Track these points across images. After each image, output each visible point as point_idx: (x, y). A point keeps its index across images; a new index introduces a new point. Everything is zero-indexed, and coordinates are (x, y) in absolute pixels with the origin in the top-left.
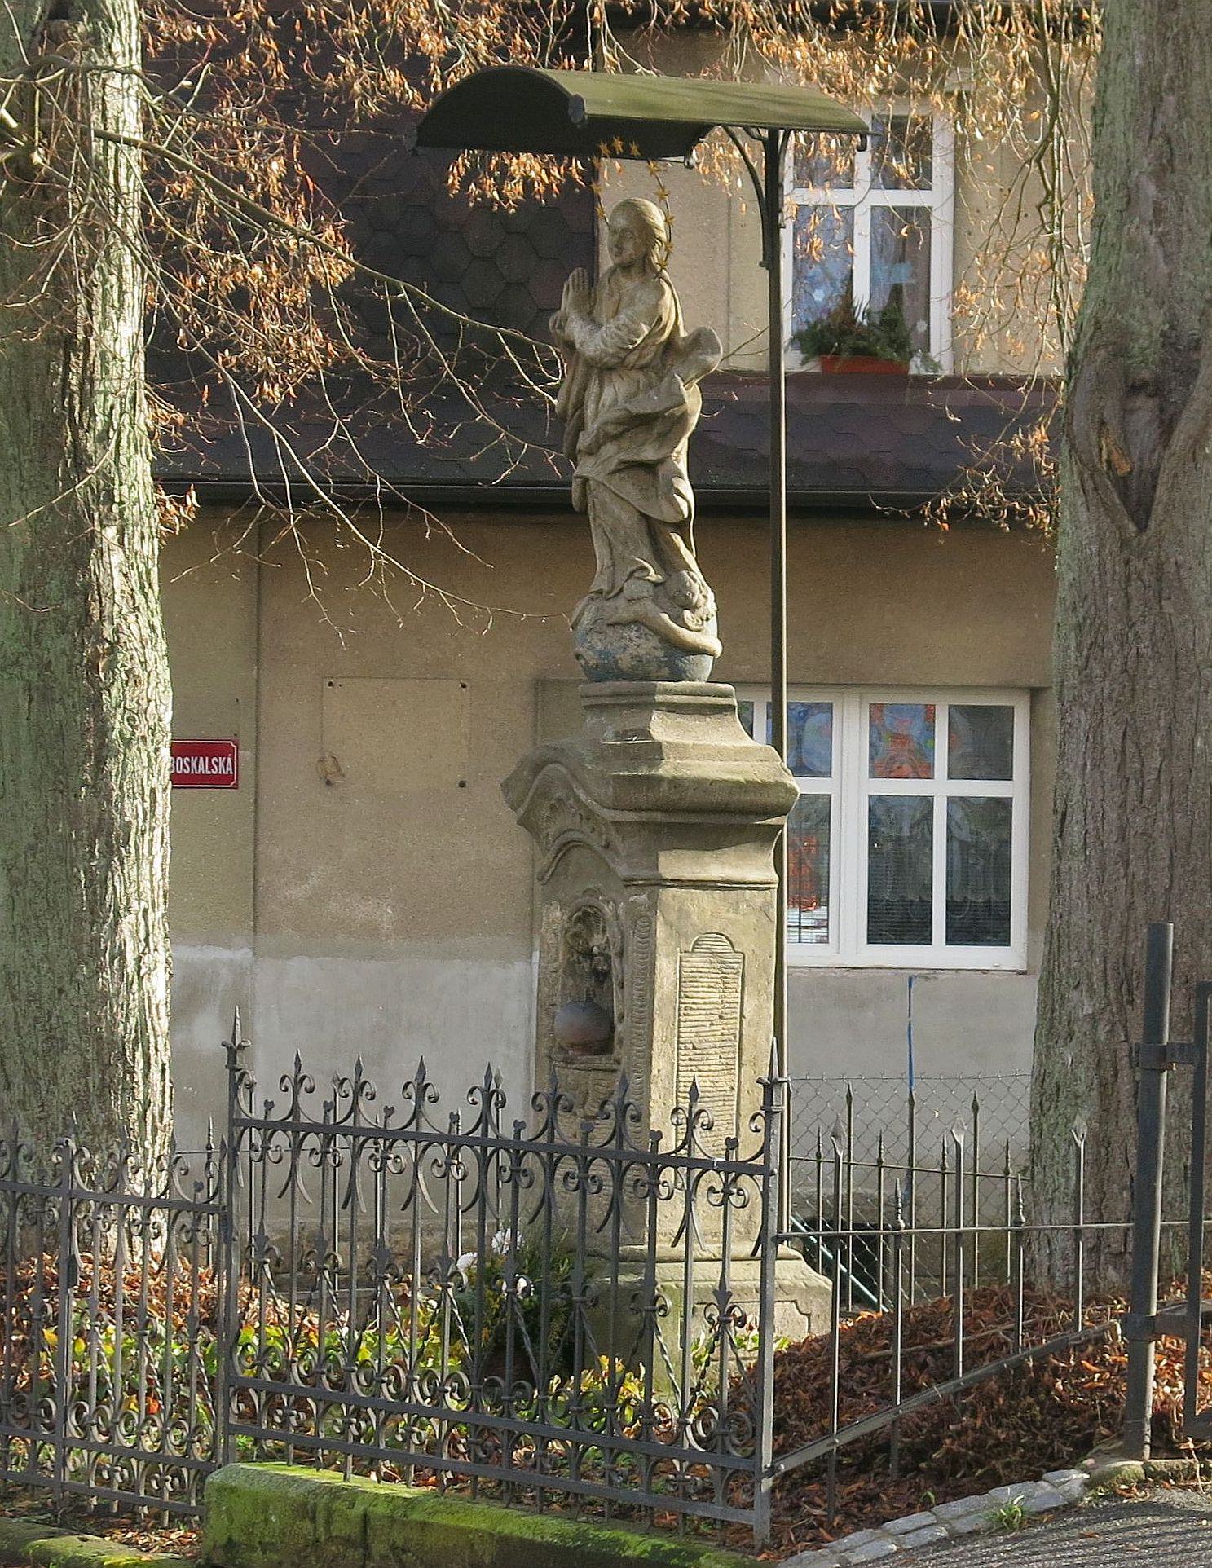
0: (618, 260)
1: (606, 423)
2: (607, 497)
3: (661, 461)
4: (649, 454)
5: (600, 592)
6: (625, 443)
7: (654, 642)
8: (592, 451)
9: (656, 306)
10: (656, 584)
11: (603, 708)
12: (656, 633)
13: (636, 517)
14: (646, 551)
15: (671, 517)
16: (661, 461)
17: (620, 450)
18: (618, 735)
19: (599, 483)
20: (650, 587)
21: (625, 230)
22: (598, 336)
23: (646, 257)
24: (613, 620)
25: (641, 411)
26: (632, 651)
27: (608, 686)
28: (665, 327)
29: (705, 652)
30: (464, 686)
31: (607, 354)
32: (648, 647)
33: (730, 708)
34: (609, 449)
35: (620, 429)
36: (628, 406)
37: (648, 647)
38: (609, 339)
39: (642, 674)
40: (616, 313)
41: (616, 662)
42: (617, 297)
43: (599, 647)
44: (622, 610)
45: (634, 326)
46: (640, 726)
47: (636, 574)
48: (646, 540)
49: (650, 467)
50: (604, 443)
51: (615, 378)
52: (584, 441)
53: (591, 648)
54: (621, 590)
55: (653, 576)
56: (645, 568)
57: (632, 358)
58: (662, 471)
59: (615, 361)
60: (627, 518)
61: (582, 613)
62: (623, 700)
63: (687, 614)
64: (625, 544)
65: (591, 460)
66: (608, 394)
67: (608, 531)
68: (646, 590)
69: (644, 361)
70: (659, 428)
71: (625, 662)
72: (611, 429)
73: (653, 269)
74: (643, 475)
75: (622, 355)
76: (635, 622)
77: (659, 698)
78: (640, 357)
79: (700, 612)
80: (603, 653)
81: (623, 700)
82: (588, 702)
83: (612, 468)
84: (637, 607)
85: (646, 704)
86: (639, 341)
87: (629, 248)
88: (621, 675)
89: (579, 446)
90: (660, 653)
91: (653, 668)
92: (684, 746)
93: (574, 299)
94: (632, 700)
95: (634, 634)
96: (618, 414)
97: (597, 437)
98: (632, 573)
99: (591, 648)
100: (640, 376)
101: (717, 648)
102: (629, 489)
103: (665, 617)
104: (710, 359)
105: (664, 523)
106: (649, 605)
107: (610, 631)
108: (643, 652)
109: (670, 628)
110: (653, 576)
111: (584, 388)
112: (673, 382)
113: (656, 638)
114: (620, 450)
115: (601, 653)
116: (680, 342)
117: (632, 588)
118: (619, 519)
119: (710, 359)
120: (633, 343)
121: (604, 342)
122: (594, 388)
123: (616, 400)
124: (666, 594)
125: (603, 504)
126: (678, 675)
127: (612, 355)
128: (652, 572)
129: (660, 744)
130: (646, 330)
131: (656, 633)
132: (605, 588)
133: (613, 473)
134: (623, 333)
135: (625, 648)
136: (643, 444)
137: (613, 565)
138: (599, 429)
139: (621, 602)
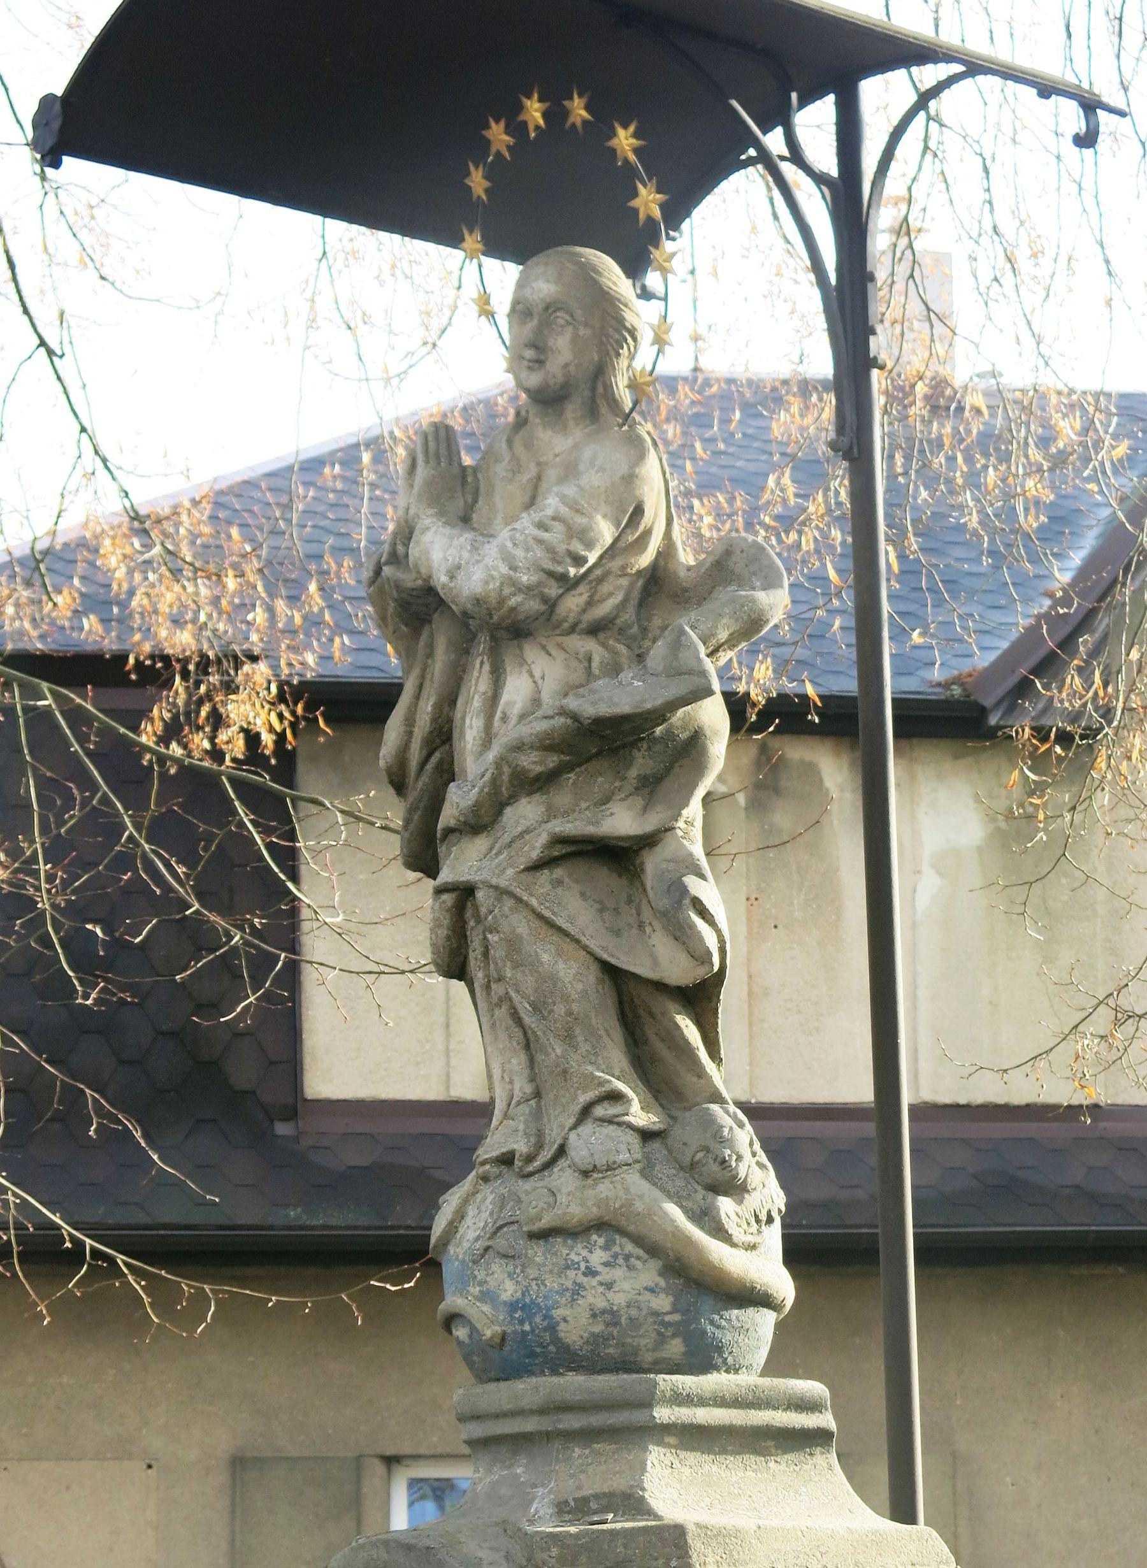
0: (534, 380)
1: (519, 747)
2: (522, 925)
3: (649, 841)
4: (622, 821)
5: (507, 1160)
6: (562, 797)
7: (649, 1274)
8: (477, 824)
9: (630, 479)
10: (647, 1135)
11: (519, 1442)
12: (653, 1250)
13: (593, 974)
14: (617, 1056)
15: (676, 969)
16: (649, 841)
17: (551, 813)
18: (574, 1508)
19: (502, 892)
20: (634, 1140)
21: (551, 307)
22: (491, 551)
23: (600, 373)
24: (545, 1222)
25: (604, 710)
26: (595, 1298)
27: (528, 1390)
28: (648, 532)
29: (752, 1297)
30: (150, 1467)
31: (513, 582)
32: (634, 1286)
33: (818, 1438)
34: (525, 812)
35: (552, 761)
36: (572, 703)
37: (634, 1286)
38: (519, 553)
39: (614, 1353)
40: (531, 502)
41: (552, 1328)
42: (533, 471)
43: (509, 1291)
44: (565, 1196)
45: (581, 521)
46: (618, 1483)
47: (599, 1111)
48: (618, 1033)
49: (620, 857)
50: (512, 799)
51: (531, 652)
52: (459, 800)
53: (486, 1296)
54: (561, 1151)
55: (640, 1115)
56: (615, 1097)
57: (573, 603)
58: (653, 863)
59: (534, 606)
60: (573, 976)
61: (460, 1214)
62: (572, 1422)
63: (725, 1205)
64: (568, 1038)
65: (480, 844)
66: (516, 690)
67: (524, 1008)
68: (627, 1147)
69: (604, 609)
70: (641, 763)
71: (575, 1326)
72: (532, 763)
73: (614, 403)
74: (604, 877)
75: (553, 590)
76: (601, 1225)
77: (663, 1414)
78: (590, 603)
79: (753, 1201)
80: (521, 1308)
81: (572, 1422)
82: (478, 1430)
83: (535, 855)
84: (605, 1189)
85: (626, 1429)
86: (592, 558)
87: (562, 346)
88: (567, 1359)
89: (448, 816)
90: (662, 1303)
91: (644, 1340)
92: (737, 1533)
93: (429, 483)
94: (596, 1420)
95: (598, 1257)
96: (541, 726)
97: (495, 782)
98: (586, 1111)
99: (486, 1296)
100: (590, 645)
101: (782, 1284)
102: (573, 903)
103: (674, 1211)
104: (762, 597)
105: (660, 987)
106: (635, 1181)
107: (537, 1252)
108: (619, 1299)
109: (689, 1241)
110: (640, 1115)
111: (450, 699)
112: (679, 642)
113: (654, 1265)
114: (551, 813)
115: (513, 1306)
116: (682, 573)
117: (589, 1143)
118: (553, 978)
119: (762, 597)
120: (579, 560)
121: (507, 557)
122: (478, 683)
123: (536, 702)
124: (673, 1157)
125: (513, 944)
126: (703, 1356)
127: (528, 590)
128: (636, 1106)
129: (678, 1533)
130: (606, 532)
131: (653, 1250)
132: (521, 1146)
133: (536, 867)
134: (555, 536)
135: (577, 1291)
136: (606, 800)
137: (538, 1094)
138: (499, 763)
139: (563, 1178)
